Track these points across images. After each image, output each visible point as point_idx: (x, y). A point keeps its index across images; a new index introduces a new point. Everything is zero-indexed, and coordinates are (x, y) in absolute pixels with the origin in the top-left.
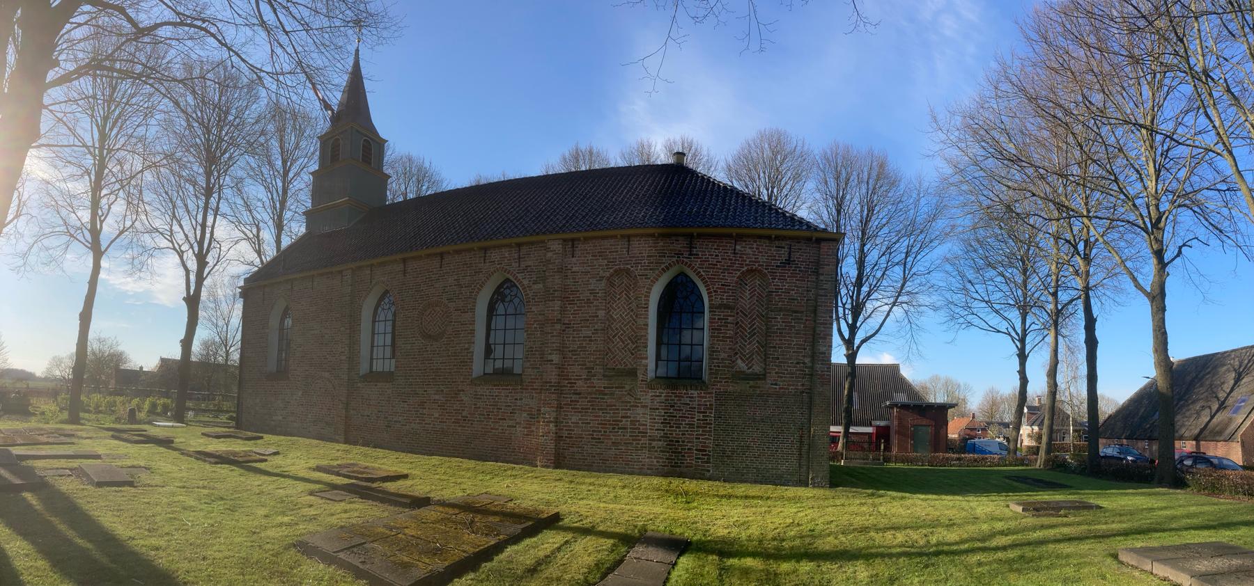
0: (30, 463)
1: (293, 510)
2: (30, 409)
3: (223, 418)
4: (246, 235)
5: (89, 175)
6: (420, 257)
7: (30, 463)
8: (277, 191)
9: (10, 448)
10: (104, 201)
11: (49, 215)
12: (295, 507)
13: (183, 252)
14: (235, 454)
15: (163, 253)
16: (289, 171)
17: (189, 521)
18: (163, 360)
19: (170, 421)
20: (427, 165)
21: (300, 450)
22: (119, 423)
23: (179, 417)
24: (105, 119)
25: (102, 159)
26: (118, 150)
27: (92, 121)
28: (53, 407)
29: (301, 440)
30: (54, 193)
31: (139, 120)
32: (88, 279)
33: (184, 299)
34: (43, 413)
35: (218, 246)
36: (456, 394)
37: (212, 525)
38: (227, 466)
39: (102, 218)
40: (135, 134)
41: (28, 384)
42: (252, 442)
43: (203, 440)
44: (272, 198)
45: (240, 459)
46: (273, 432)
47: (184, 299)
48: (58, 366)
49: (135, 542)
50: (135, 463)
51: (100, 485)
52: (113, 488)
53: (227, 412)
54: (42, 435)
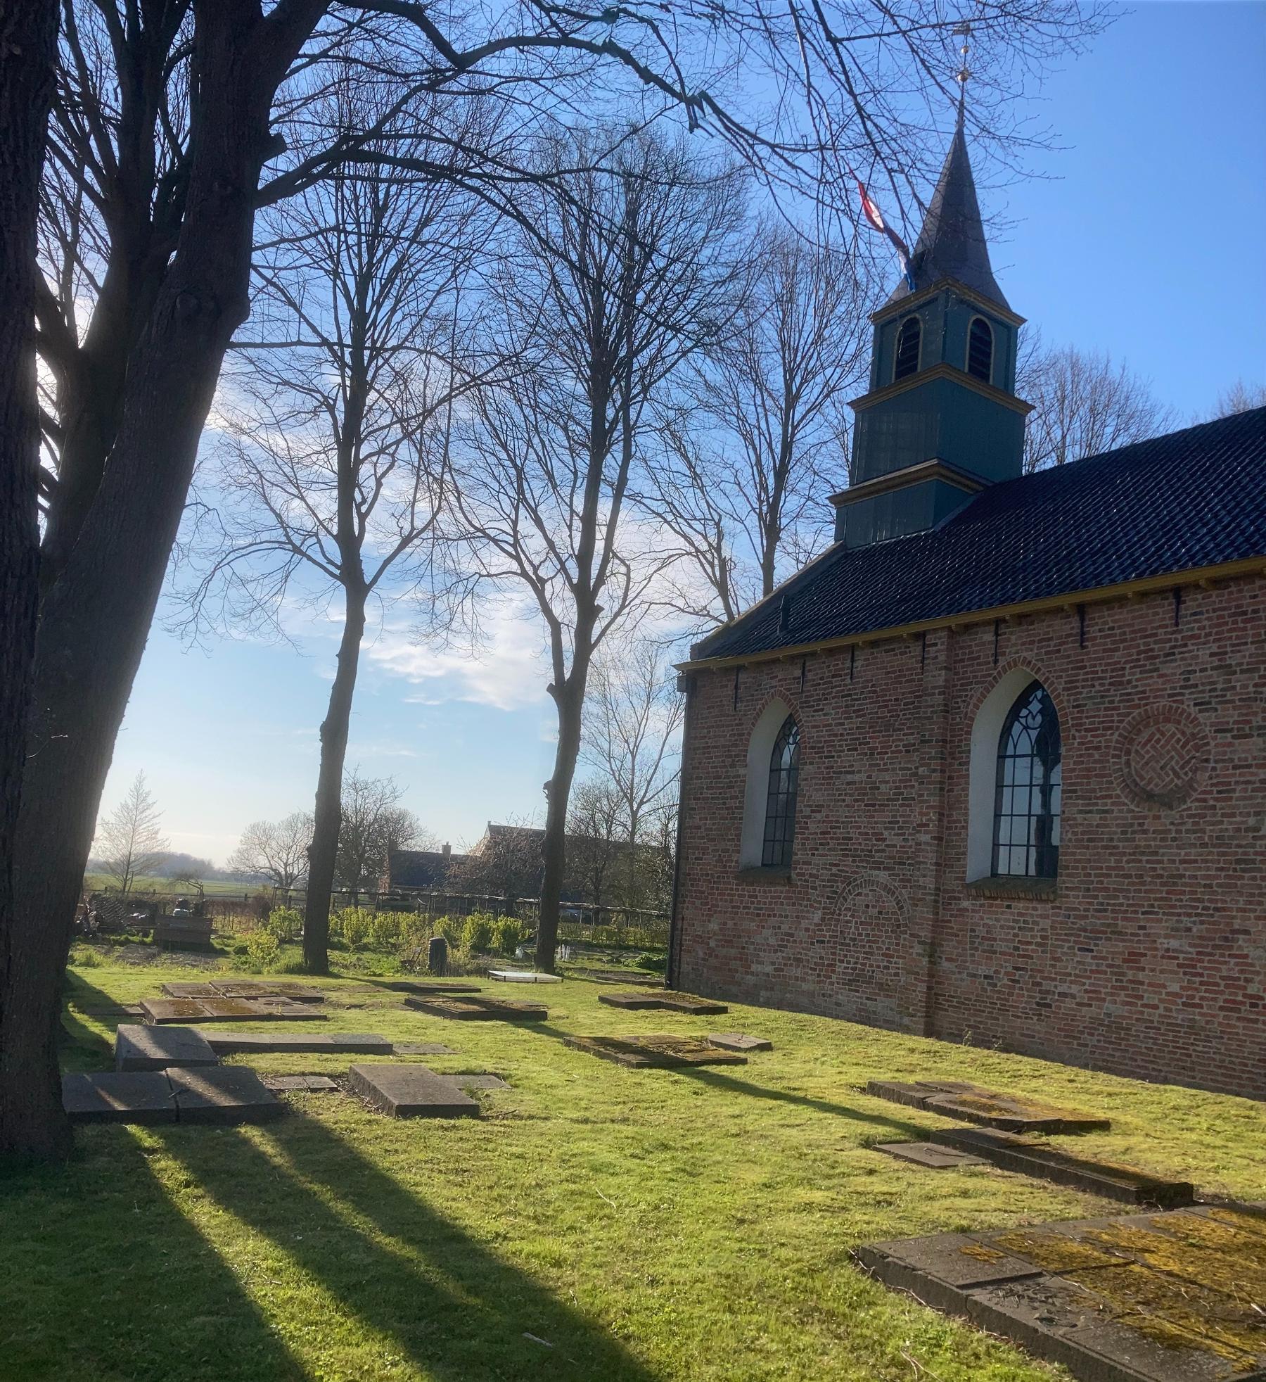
0: (241, 1060)
1: (829, 1177)
2: (215, 942)
3: (631, 963)
4: (692, 544)
5: (331, 409)
6: (1121, 600)
7: (241, 1060)
8: (770, 445)
9: (194, 1027)
10: (365, 470)
11: (244, 507)
12: (832, 1171)
13: (543, 582)
14: (676, 1045)
15: (499, 590)
16: (798, 396)
17: (610, 1196)
18: (494, 830)
19: (521, 968)
20: (1115, 373)
21: (821, 1044)
22: (411, 971)
23: (545, 962)
24: (364, 280)
25: (359, 370)
26: (395, 349)
27: (335, 285)
28: (265, 938)
29: (820, 1021)
30: (256, 453)
31: (440, 280)
32: (338, 647)
33: (551, 689)
34: (242, 951)
35: (623, 569)
36: (1226, 939)
37: (656, 1208)
38: (663, 1072)
39: (364, 509)
40: (433, 312)
41: (201, 887)
42: (703, 1017)
43: (605, 1013)
44: (759, 462)
45: (689, 1057)
46: (751, 999)
47: (551, 689)
48: (262, 846)
49: (511, 1246)
50: (474, 1064)
51: (406, 1112)
52: (437, 1121)
53: (637, 949)
54: (255, 998)
